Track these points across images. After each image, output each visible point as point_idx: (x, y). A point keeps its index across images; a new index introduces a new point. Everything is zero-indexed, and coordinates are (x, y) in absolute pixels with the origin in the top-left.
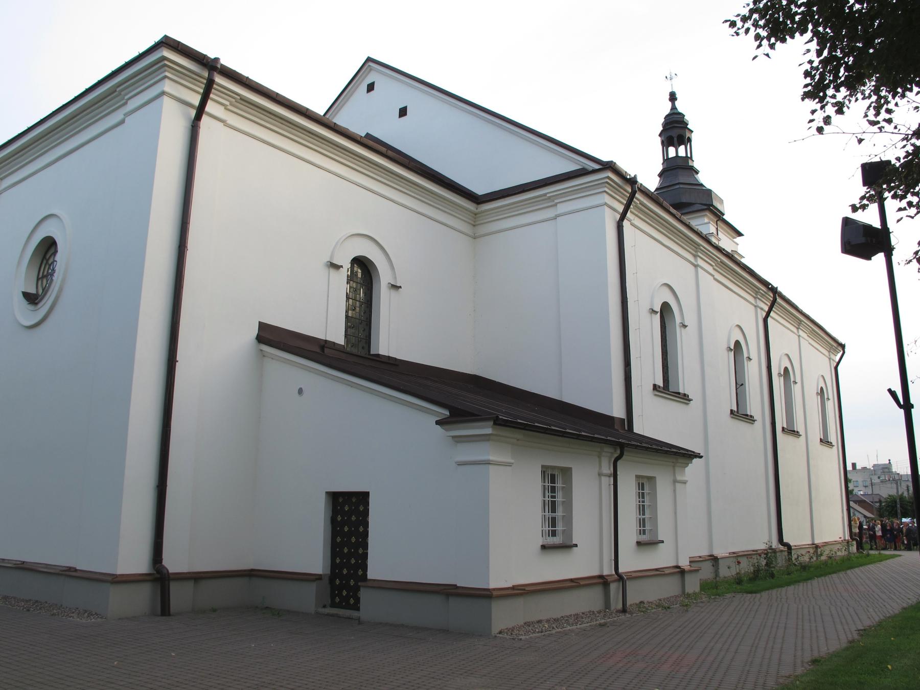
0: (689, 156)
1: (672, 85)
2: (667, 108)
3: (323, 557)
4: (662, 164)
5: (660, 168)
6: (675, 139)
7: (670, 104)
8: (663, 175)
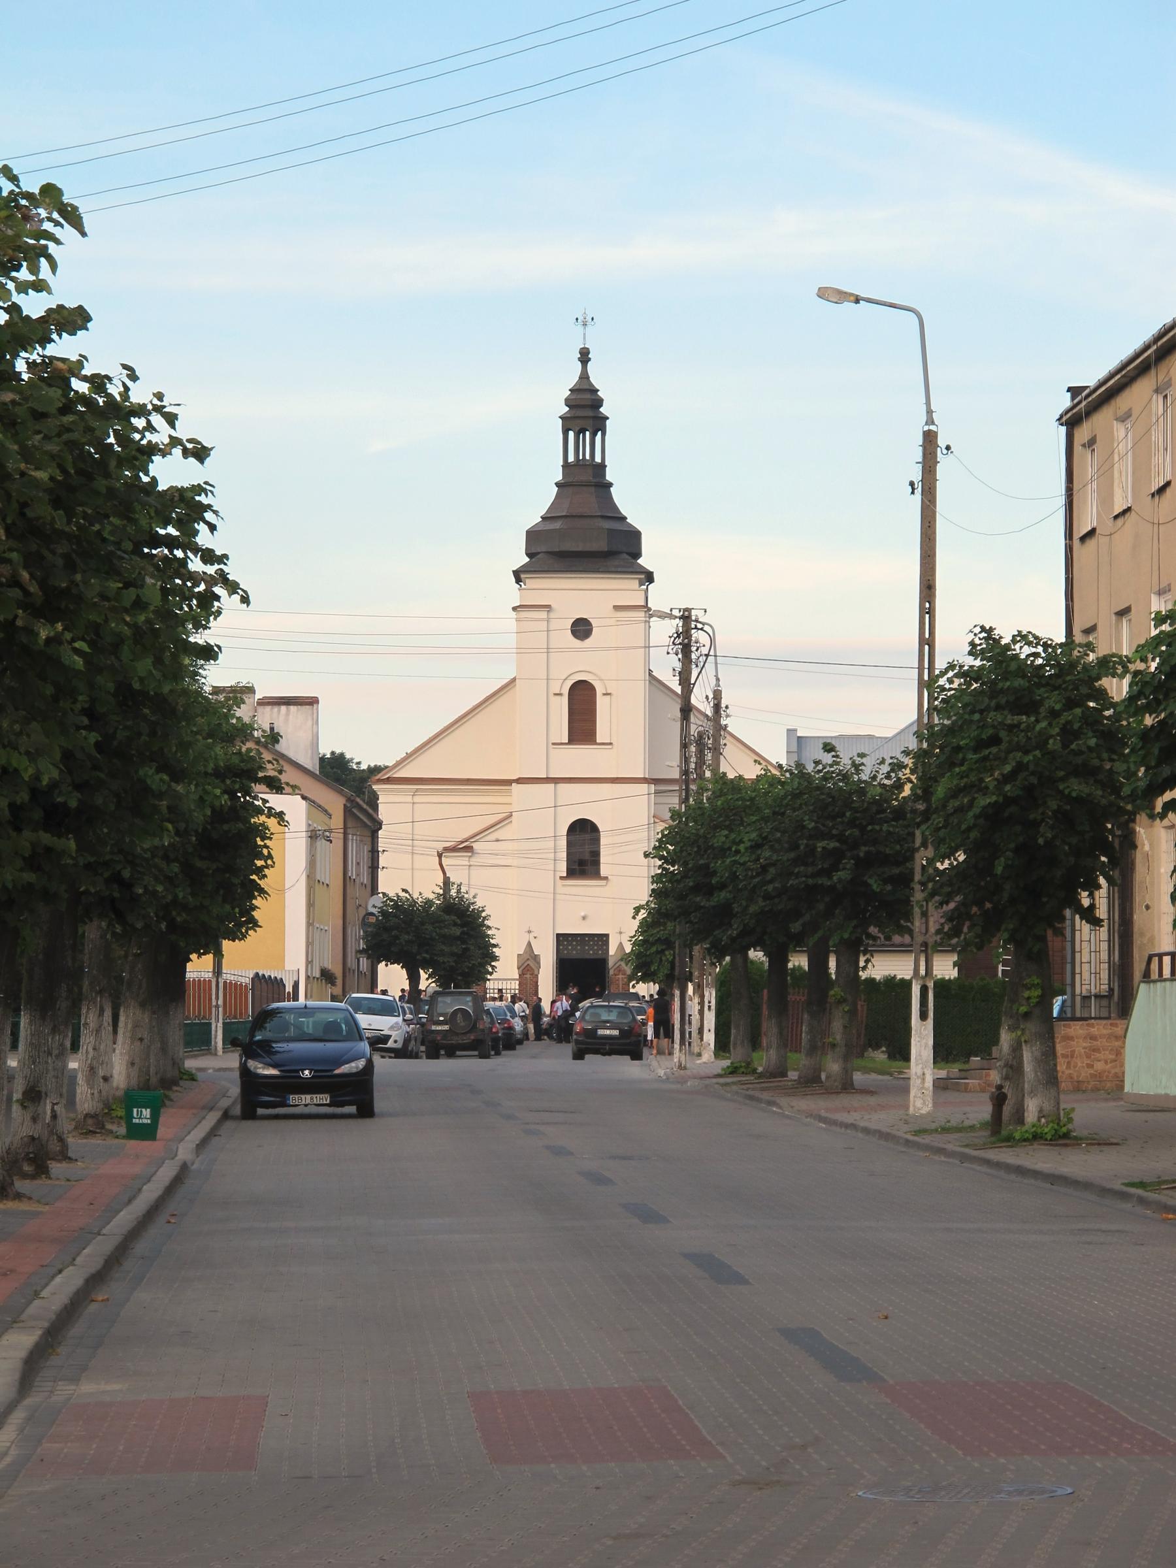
0: (571, 434)
1: (584, 334)
2: (573, 379)
3: (1132, 936)
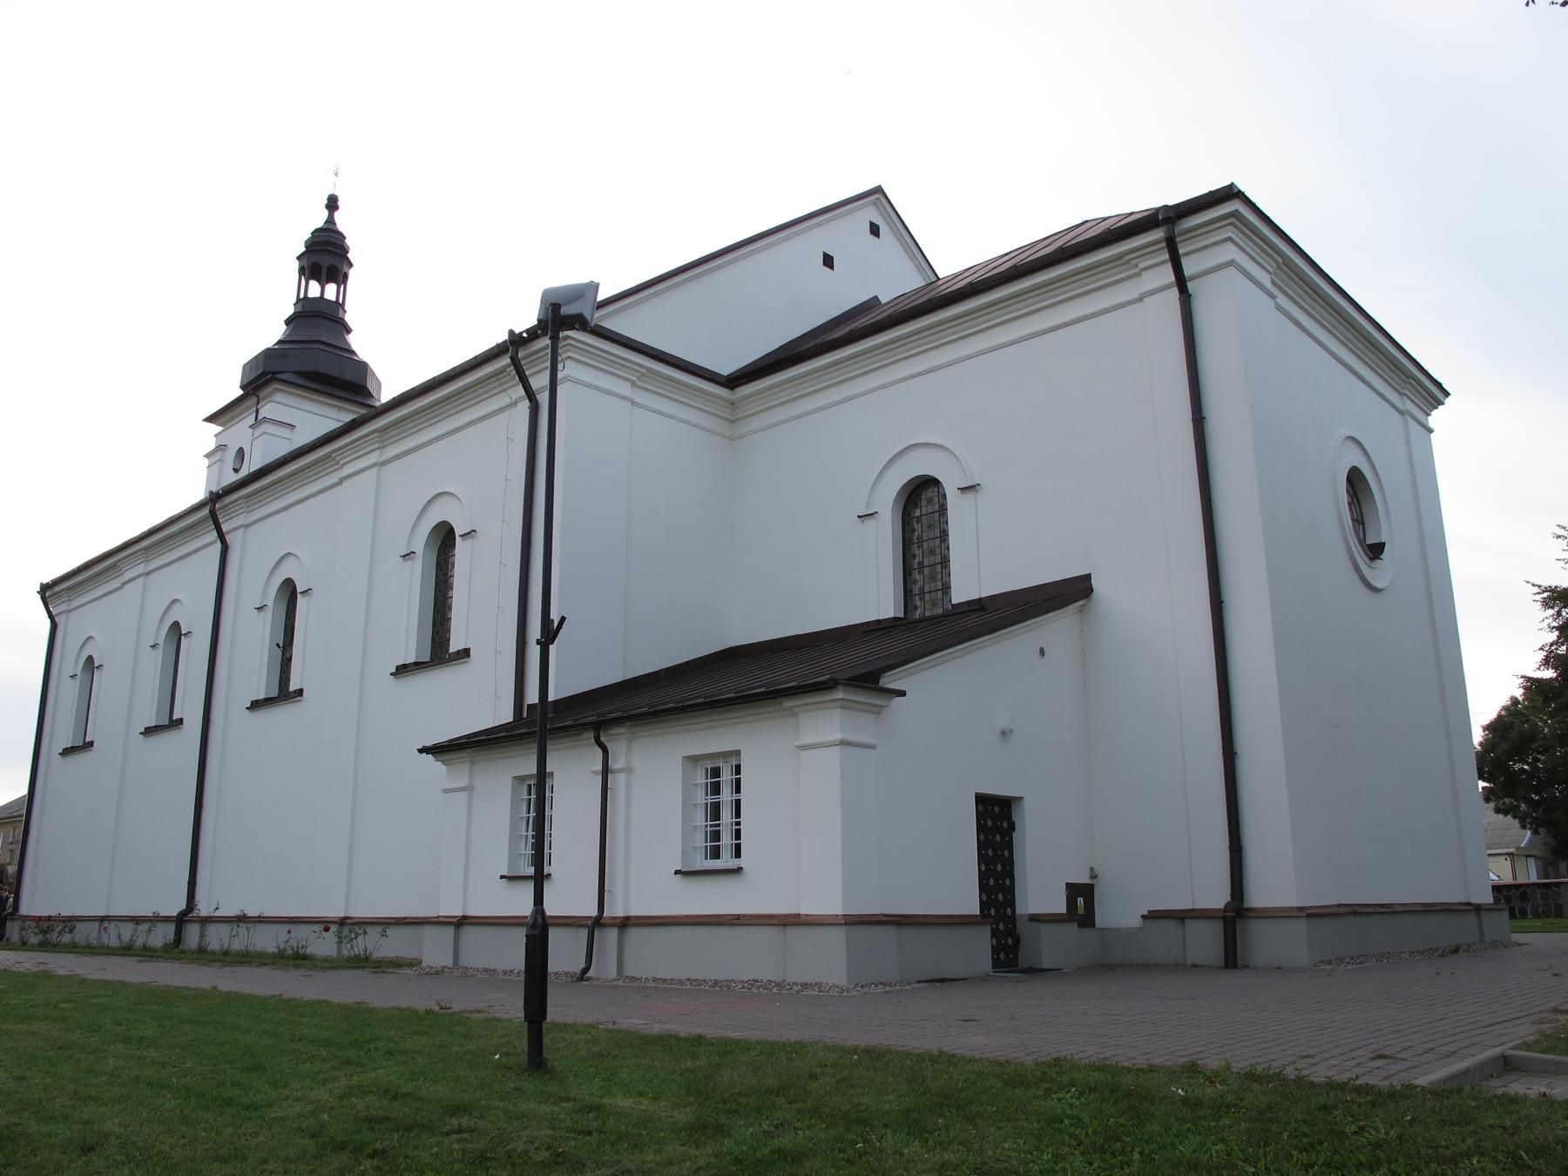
0: (341, 301)
2: (319, 219)
4: (295, 305)
5: (290, 311)
6: (324, 270)
7: (325, 213)
8: (293, 323)
